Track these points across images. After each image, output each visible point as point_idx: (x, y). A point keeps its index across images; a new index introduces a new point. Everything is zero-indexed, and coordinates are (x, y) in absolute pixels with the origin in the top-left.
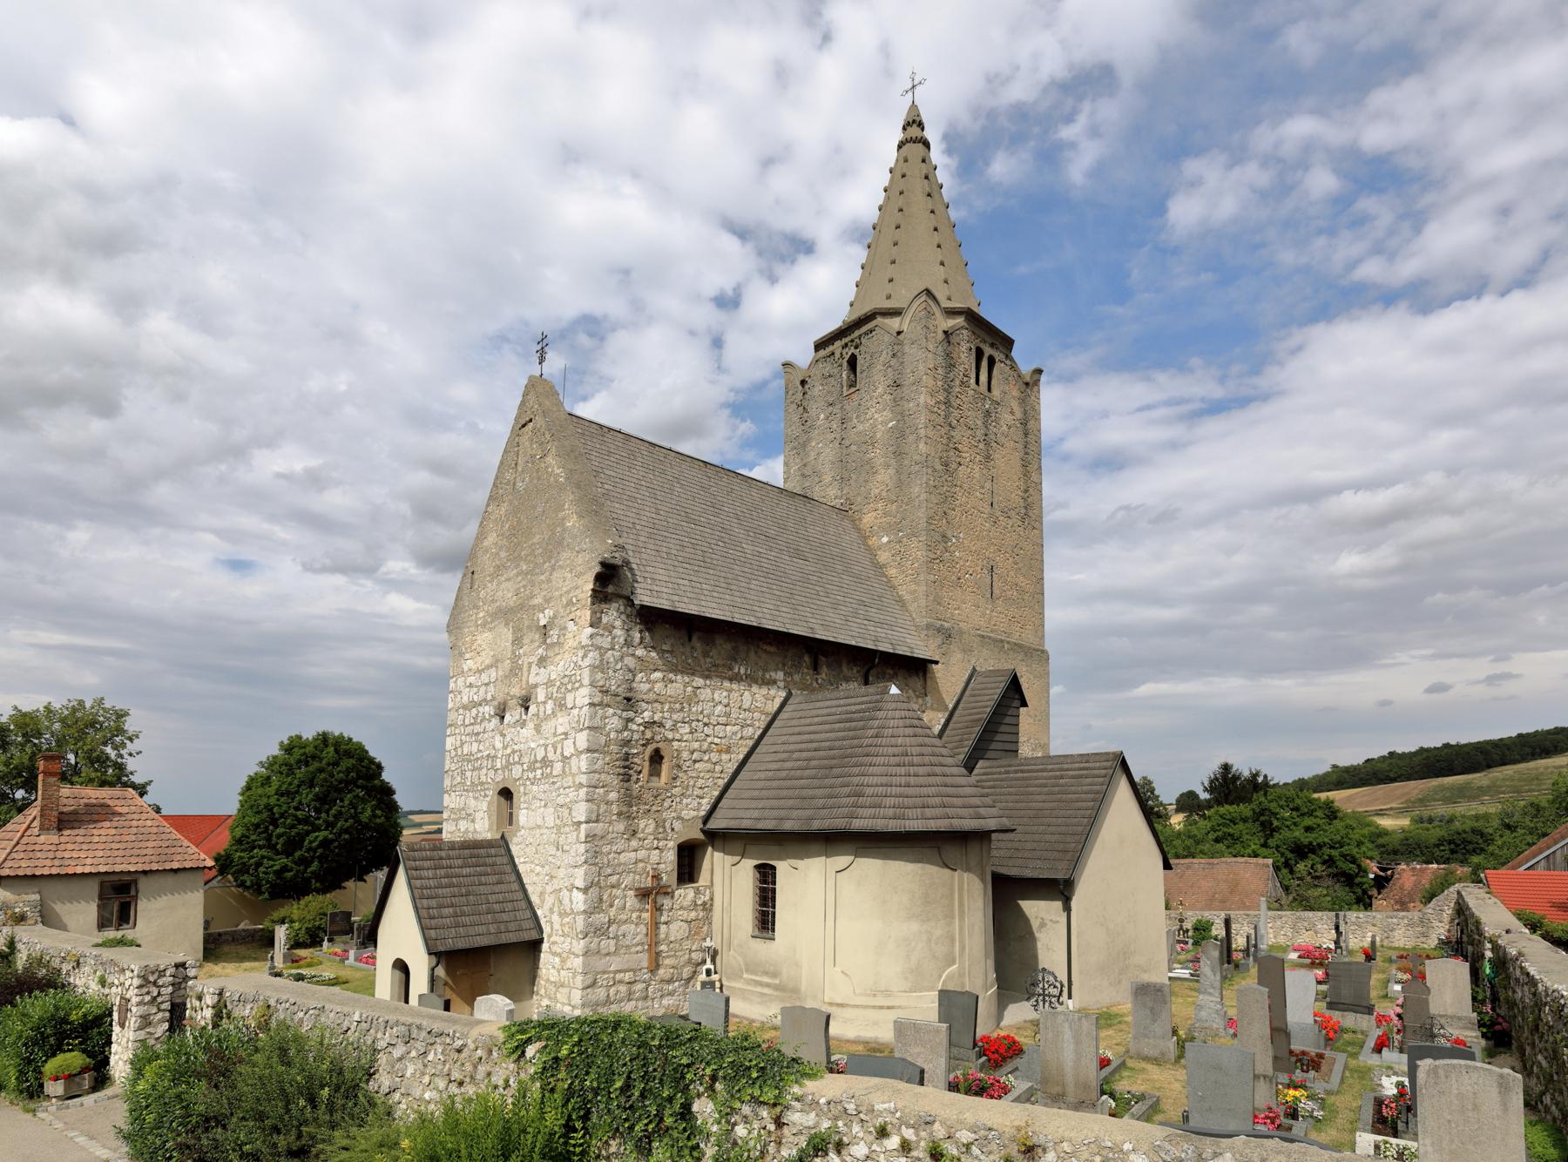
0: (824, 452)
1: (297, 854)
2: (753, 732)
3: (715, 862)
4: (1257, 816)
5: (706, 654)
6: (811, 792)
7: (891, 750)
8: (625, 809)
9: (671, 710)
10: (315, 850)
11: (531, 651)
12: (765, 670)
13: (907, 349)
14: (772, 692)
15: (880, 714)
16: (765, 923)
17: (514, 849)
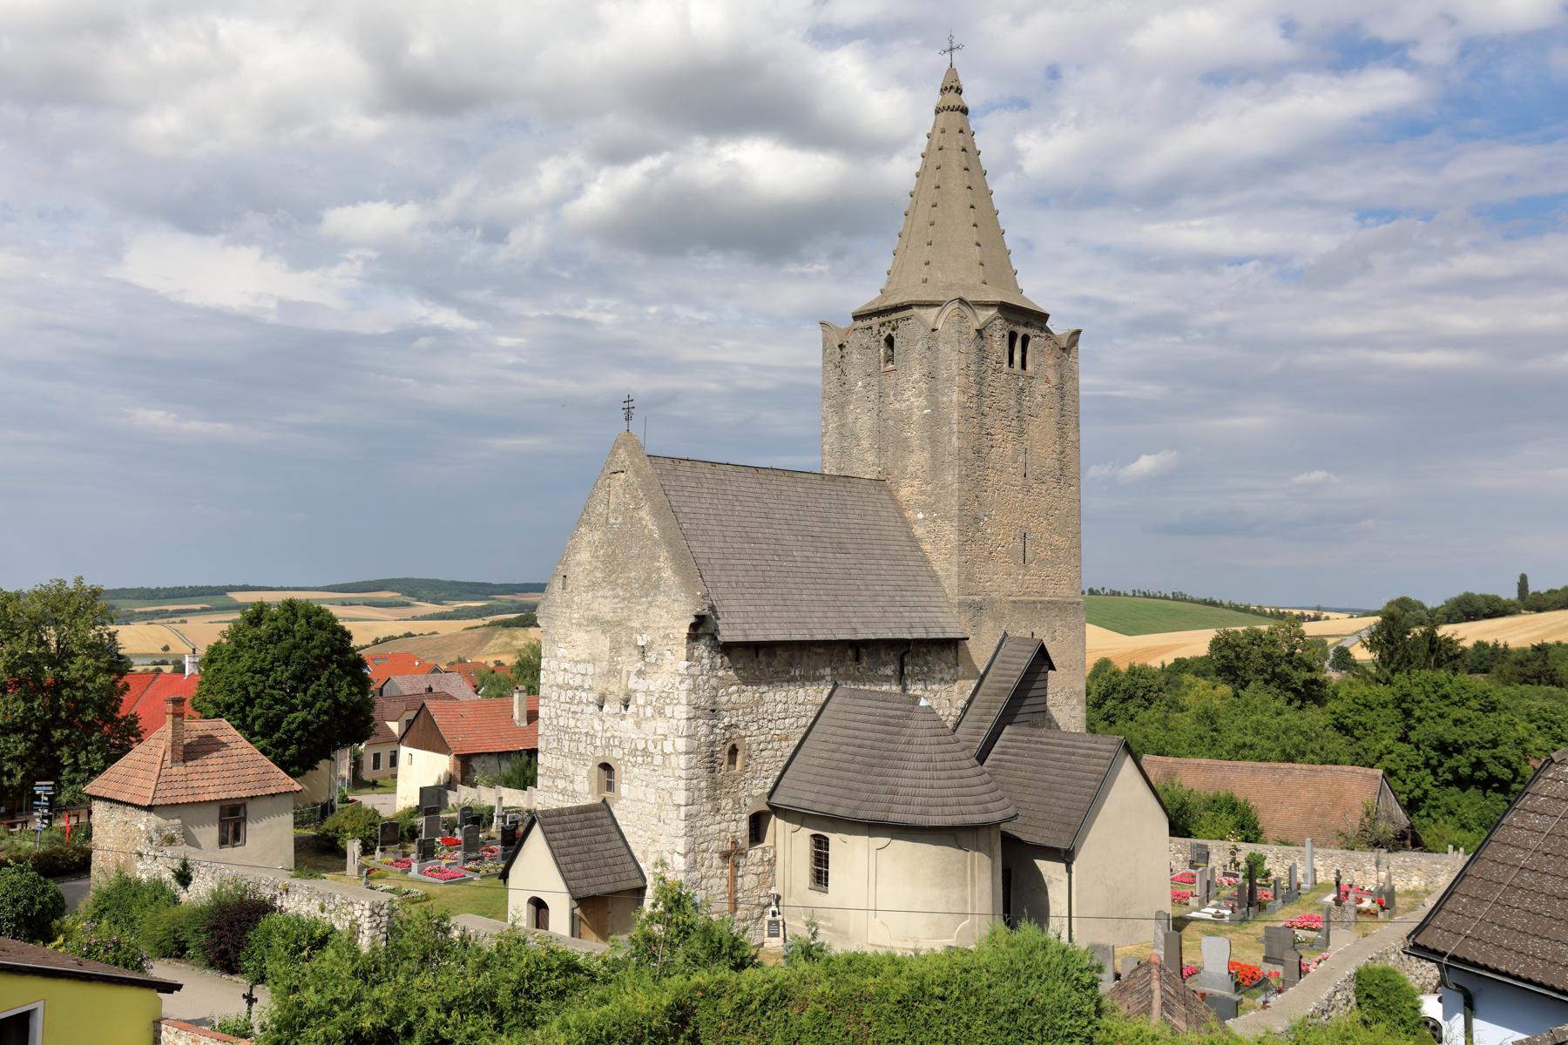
0: (862, 419)
1: (276, 736)
3: (778, 828)
4: (1400, 701)
5: (769, 665)
6: (857, 785)
7: (920, 757)
9: (744, 714)
10: (293, 732)
11: (629, 662)
12: (816, 669)
13: (941, 345)
15: (912, 723)
16: (820, 877)
17: (616, 813)
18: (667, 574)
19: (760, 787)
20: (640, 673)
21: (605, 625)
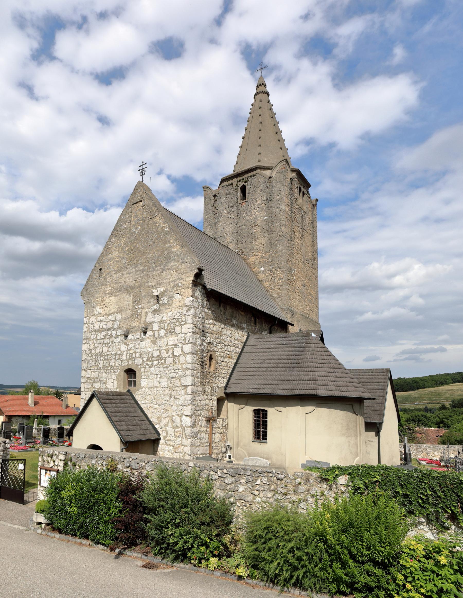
2: (238, 350)
8: (202, 381)
11: (147, 307)
13: (274, 185)
14: (244, 333)
17: (137, 397)
18: (176, 249)
19: (222, 382)
20: (155, 312)
21: (128, 289)
